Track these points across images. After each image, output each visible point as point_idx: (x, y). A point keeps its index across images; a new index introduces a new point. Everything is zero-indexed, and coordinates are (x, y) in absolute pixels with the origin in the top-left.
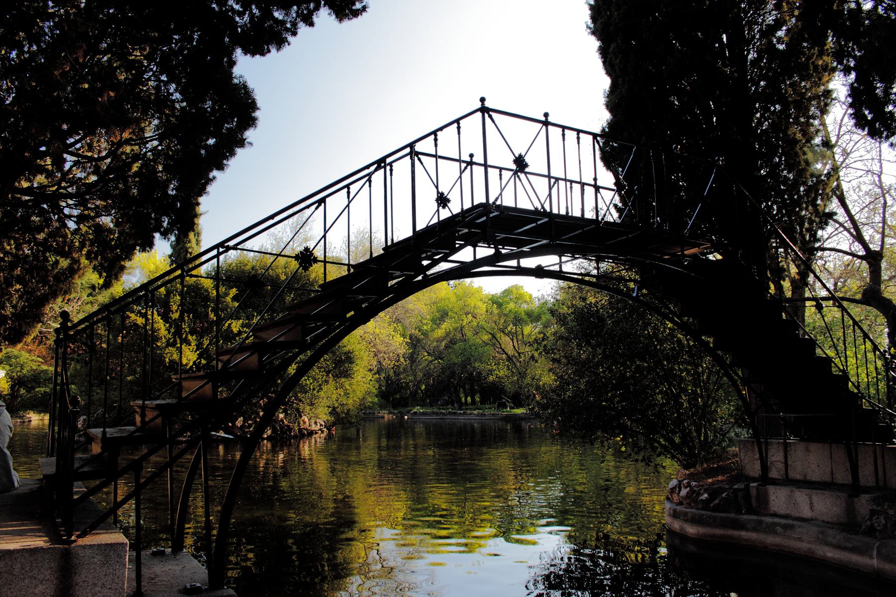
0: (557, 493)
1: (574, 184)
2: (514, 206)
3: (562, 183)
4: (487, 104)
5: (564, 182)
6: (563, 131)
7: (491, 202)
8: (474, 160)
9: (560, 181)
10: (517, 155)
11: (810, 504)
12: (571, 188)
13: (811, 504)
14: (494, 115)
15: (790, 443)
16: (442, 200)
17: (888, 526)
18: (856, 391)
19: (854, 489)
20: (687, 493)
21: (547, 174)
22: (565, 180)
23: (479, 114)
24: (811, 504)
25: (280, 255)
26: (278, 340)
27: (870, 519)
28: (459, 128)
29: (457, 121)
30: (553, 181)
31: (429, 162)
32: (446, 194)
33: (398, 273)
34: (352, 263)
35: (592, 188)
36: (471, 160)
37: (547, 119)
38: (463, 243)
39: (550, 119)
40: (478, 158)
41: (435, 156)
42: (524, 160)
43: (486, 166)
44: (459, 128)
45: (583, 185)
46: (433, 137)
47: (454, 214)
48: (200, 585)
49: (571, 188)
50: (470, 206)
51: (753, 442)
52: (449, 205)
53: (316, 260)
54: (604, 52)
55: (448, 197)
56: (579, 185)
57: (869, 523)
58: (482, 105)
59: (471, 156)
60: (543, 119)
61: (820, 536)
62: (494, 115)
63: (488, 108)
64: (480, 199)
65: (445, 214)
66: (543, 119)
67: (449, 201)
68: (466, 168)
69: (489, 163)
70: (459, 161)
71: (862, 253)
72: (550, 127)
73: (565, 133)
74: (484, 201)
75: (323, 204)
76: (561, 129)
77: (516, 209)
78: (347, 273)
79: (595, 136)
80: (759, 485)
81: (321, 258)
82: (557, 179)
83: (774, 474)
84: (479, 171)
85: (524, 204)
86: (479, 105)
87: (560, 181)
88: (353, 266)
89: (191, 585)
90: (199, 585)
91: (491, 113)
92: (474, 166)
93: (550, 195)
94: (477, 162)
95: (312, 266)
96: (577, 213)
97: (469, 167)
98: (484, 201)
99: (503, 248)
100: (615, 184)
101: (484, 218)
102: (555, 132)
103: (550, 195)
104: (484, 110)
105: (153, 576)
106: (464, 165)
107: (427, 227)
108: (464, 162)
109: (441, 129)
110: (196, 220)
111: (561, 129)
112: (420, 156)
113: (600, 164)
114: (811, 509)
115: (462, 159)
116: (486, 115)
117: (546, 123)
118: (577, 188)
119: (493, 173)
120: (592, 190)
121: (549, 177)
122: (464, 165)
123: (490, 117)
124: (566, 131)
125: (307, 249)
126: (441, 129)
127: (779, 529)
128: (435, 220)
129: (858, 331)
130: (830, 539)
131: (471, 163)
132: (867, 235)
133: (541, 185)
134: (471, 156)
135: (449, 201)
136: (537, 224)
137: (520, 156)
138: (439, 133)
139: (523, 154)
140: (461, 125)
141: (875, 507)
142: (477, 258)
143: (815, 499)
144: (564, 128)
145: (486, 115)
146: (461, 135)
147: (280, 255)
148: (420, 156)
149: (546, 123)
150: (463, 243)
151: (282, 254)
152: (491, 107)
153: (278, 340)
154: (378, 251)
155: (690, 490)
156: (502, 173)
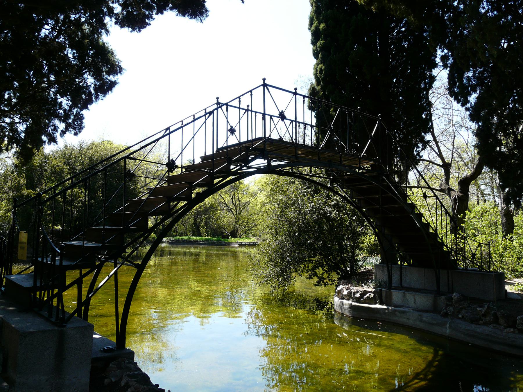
1: (300, 124)
4: (266, 82)
5: (251, 112)
7: (267, 136)
10: (281, 112)
11: (414, 300)
12: (256, 116)
13: (415, 300)
15: (404, 267)
16: (232, 131)
17: (455, 312)
18: (440, 241)
19: (438, 293)
21: (239, 107)
23: (262, 87)
24: (415, 300)
25: (143, 160)
27: (446, 309)
28: (251, 95)
29: (251, 91)
34: (184, 165)
37: (296, 91)
38: (254, 157)
39: (298, 91)
42: (284, 114)
44: (251, 95)
45: (305, 124)
49: (256, 116)
50: (255, 138)
51: (383, 267)
52: (235, 133)
53: (177, 167)
55: (235, 129)
56: (303, 125)
57: (445, 311)
60: (294, 91)
61: (420, 317)
64: (260, 135)
66: (294, 91)
71: (441, 163)
72: (297, 96)
79: (304, 97)
80: (387, 290)
81: (180, 165)
82: (299, 123)
83: (394, 285)
84: (294, 123)
88: (184, 167)
95: (175, 170)
96: (301, 142)
97: (247, 112)
100: (73, 57)
104: (265, 85)
109: (242, 95)
114: (415, 303)
117: (295, 94)
118: (302, 126)
123: (268, 89)
126: (242, 95)
127: (397, 313)
129: (443, 209)
130: (424, 319)
131: (247, 110)
132: (444, 155)
137: (282, 112)
140: (252, 93)
141: (448, 303)
143: (417, 298)
145: (266, 88)
147: (143, 160)
149: (295, 94)
150: (254, 157)
151: (145, 160)
152: (268, 83)
154: (198, 161)
156: (257, 115)
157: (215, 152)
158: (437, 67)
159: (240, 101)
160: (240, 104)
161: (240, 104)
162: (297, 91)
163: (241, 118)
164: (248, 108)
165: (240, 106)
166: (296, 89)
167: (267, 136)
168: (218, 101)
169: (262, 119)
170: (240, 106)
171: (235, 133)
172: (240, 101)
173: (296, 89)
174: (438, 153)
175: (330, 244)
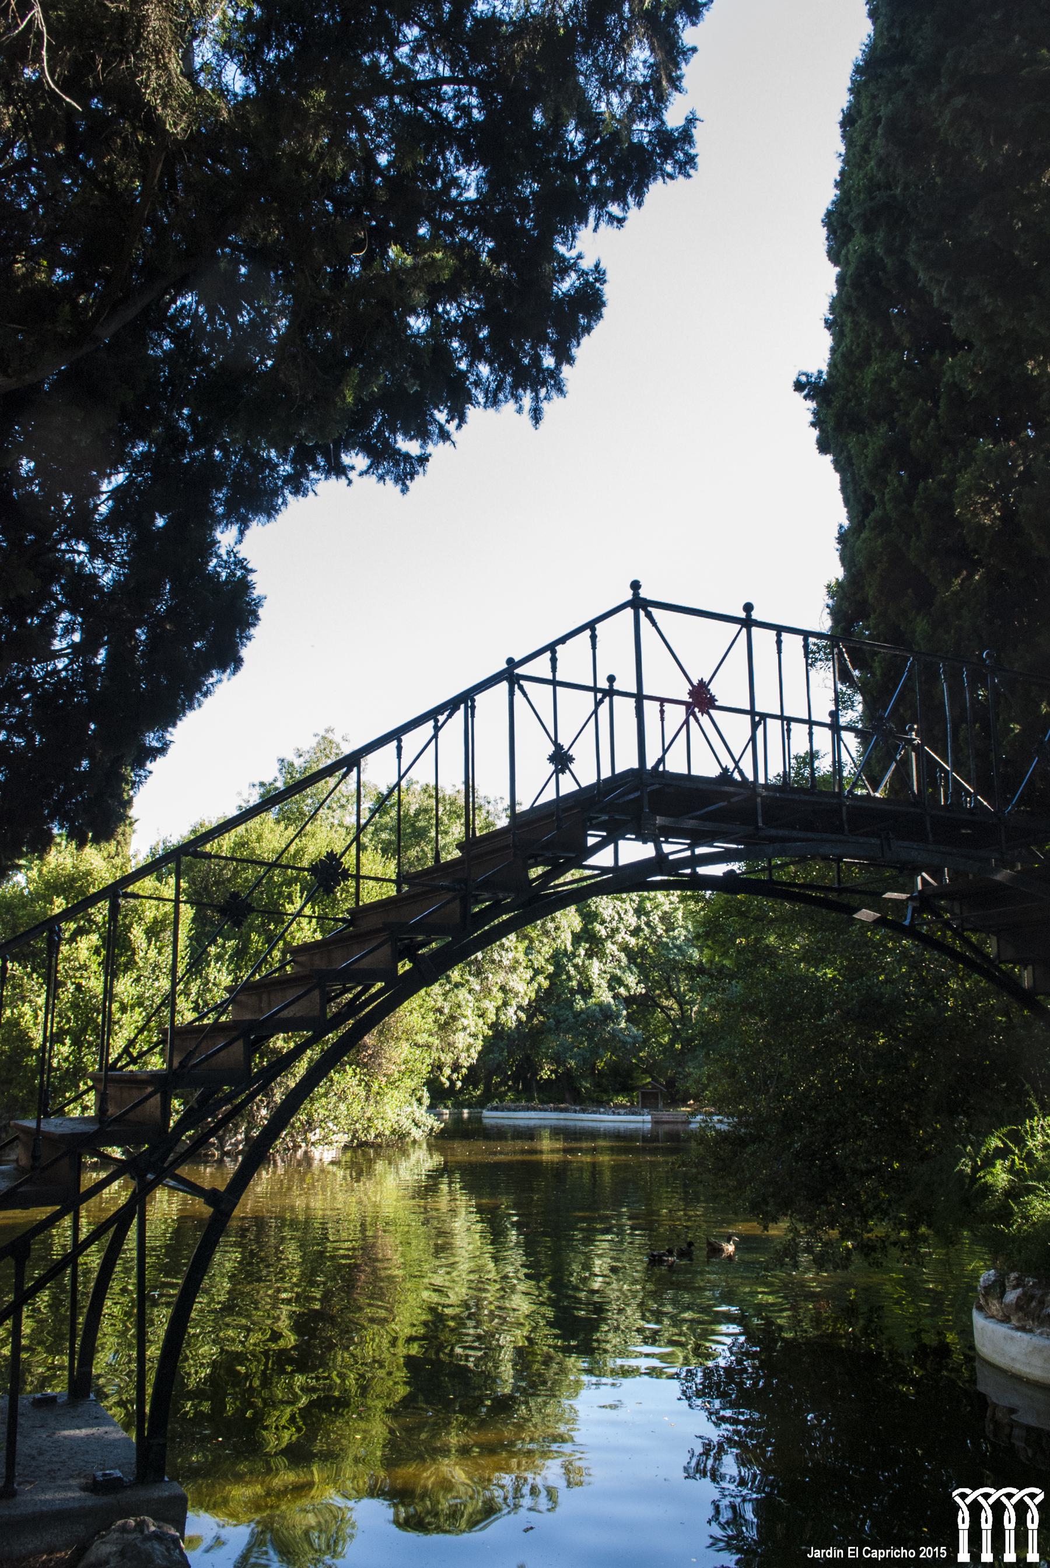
0: (456, 1225)
2: (686, 772)
3: (774, 726)
4: (643, 593)
6: (779, 635)
7: (650, 764)
8: (617, 686)
9: (768, 720)
10: (695, 682)
14: (656, 612)
16: (561, 760)
20: (1018, 1298)
22: (781, 717)
23: (629, 612)
26: (282, 1015)
28: (593, 637)
29: (591, 625)
30: (757, 718)
31: (541, 694)
32: (566, 748)
33: (486, 895)
35: (827, 729)
36: (611, 686)
37: (749, 615)
39: (755, 615)
40: (626, 683)
41: (554, 683)
43: (640, 698)
44: (593, 637)
45: (787, 721)
46: (548, 655)
47: (583, 785)
48: (120, 1474)
53: (345, 875)
54: (844, 489)
55: (570, 752)
58: (634, 595)
59: (611, 679)
60: (742, 615)
62: (656, 612)
63: (645, 600)
64: (627, 761)
65: (568, 786)
66: (742, 615)
67: (571, 759)
68: (601, 701)
69: (645, 692)
70: (594, 689)
72: (754, 630)
73: (782, 638)
74: (636, 766)
75: (355, 769)
76: (775, 632)
77: (689, 777)
78: (395, 893)
81: (353, 871)
82: (764, 716)
84: (625, 707)
85: (706, 767)
86: (629, 595)
87: (768, 720)
89: (105, 1475)
90: (118, 1473)
91: (650, 609)
92: (616, 699)
93: (753, 739)
94: (621, 689)
97: (607, 700)
98: (636, 766)
99: (667, 842)
101: (637, 794)
102: (763, 638)
103: (753, 739)
104: (638, 604)
105: (34, 1452)
106: (599, 696)
107: (532, 808)
108: (601, 690)
109: (563, 640)
110: (128, 793)
111: (775, 632)
112: (522, 682)
113: (838, 682)
115: (598, 686)
116: (642, 613)
117: (748, 623)
119: (651, 708)
120: (827, 733)
121: (752, 712)
122: (599, 696)
123: (649, 615)
124: (785, 636)
125: (331, 855)
126: (563, 640)
128: (549, 795)
131: (610, 693)
133: (737, 728)
134: (611, 679)
135: (571, 759)
136: (729, 802)
138: (559, 648)
139: (706, 680)
142: (561, 794)
144: (780, 629)
145: (642, 613)
146: (597, 651)
148: (522, 682)
149: (748, 623)
153: (282, 1015)
155: (1024, 1294)
157: (671, 857)
158: (338, 476)
159: (554, 660)
160: (554, 669)
161: (554, 669)
162: (753, 613)
163: (685, 726)
164: (611, 686)
165: (554, 676)
166: (748, 608)
167: (650, 764)
168: (636, 594)
169: (634, 711)
170: (554, 676)
171: (571, 766)
172: (554, 660)
173: (748, 608)
174: (447, 713)
175: (511, 1070)
